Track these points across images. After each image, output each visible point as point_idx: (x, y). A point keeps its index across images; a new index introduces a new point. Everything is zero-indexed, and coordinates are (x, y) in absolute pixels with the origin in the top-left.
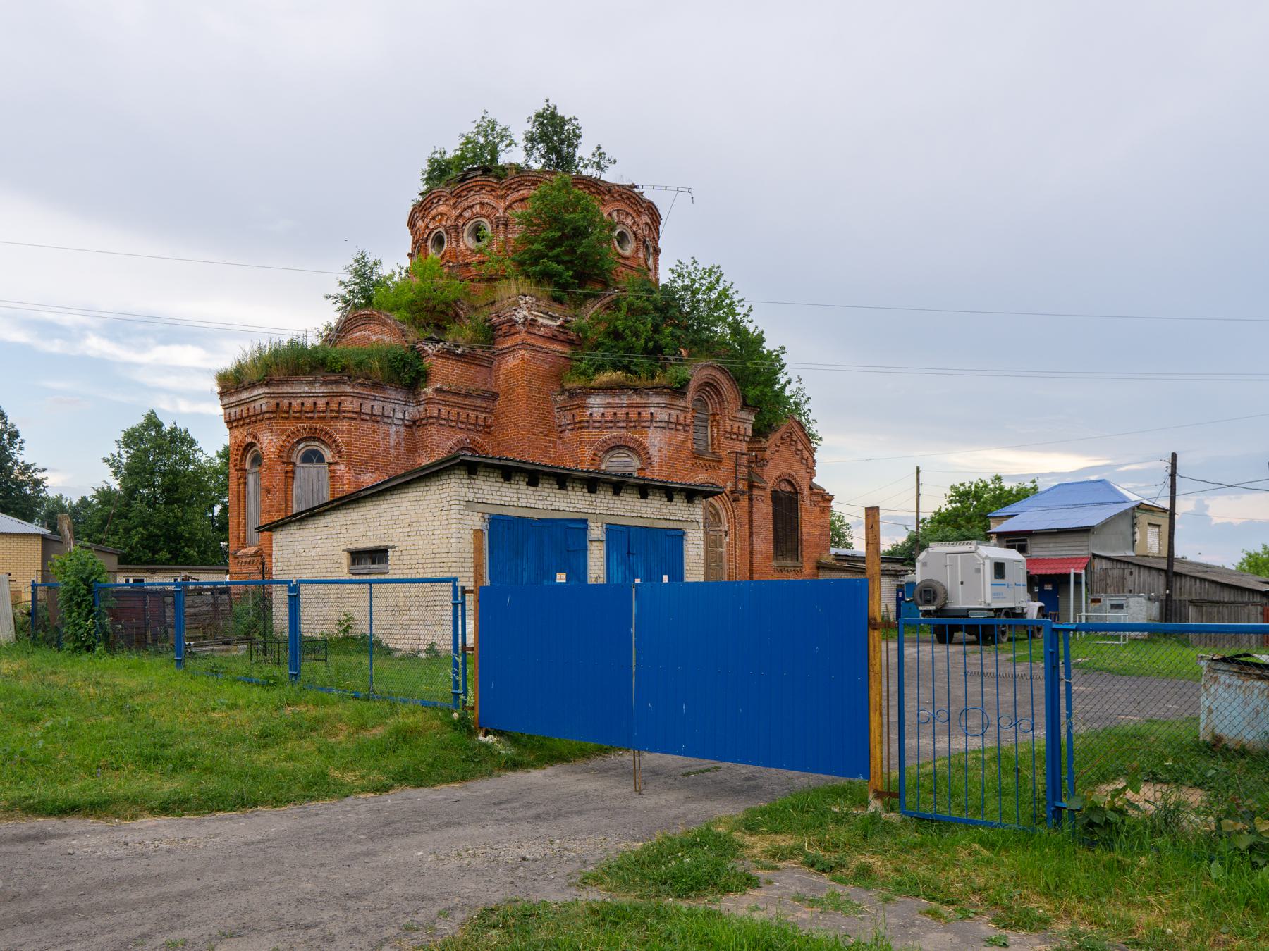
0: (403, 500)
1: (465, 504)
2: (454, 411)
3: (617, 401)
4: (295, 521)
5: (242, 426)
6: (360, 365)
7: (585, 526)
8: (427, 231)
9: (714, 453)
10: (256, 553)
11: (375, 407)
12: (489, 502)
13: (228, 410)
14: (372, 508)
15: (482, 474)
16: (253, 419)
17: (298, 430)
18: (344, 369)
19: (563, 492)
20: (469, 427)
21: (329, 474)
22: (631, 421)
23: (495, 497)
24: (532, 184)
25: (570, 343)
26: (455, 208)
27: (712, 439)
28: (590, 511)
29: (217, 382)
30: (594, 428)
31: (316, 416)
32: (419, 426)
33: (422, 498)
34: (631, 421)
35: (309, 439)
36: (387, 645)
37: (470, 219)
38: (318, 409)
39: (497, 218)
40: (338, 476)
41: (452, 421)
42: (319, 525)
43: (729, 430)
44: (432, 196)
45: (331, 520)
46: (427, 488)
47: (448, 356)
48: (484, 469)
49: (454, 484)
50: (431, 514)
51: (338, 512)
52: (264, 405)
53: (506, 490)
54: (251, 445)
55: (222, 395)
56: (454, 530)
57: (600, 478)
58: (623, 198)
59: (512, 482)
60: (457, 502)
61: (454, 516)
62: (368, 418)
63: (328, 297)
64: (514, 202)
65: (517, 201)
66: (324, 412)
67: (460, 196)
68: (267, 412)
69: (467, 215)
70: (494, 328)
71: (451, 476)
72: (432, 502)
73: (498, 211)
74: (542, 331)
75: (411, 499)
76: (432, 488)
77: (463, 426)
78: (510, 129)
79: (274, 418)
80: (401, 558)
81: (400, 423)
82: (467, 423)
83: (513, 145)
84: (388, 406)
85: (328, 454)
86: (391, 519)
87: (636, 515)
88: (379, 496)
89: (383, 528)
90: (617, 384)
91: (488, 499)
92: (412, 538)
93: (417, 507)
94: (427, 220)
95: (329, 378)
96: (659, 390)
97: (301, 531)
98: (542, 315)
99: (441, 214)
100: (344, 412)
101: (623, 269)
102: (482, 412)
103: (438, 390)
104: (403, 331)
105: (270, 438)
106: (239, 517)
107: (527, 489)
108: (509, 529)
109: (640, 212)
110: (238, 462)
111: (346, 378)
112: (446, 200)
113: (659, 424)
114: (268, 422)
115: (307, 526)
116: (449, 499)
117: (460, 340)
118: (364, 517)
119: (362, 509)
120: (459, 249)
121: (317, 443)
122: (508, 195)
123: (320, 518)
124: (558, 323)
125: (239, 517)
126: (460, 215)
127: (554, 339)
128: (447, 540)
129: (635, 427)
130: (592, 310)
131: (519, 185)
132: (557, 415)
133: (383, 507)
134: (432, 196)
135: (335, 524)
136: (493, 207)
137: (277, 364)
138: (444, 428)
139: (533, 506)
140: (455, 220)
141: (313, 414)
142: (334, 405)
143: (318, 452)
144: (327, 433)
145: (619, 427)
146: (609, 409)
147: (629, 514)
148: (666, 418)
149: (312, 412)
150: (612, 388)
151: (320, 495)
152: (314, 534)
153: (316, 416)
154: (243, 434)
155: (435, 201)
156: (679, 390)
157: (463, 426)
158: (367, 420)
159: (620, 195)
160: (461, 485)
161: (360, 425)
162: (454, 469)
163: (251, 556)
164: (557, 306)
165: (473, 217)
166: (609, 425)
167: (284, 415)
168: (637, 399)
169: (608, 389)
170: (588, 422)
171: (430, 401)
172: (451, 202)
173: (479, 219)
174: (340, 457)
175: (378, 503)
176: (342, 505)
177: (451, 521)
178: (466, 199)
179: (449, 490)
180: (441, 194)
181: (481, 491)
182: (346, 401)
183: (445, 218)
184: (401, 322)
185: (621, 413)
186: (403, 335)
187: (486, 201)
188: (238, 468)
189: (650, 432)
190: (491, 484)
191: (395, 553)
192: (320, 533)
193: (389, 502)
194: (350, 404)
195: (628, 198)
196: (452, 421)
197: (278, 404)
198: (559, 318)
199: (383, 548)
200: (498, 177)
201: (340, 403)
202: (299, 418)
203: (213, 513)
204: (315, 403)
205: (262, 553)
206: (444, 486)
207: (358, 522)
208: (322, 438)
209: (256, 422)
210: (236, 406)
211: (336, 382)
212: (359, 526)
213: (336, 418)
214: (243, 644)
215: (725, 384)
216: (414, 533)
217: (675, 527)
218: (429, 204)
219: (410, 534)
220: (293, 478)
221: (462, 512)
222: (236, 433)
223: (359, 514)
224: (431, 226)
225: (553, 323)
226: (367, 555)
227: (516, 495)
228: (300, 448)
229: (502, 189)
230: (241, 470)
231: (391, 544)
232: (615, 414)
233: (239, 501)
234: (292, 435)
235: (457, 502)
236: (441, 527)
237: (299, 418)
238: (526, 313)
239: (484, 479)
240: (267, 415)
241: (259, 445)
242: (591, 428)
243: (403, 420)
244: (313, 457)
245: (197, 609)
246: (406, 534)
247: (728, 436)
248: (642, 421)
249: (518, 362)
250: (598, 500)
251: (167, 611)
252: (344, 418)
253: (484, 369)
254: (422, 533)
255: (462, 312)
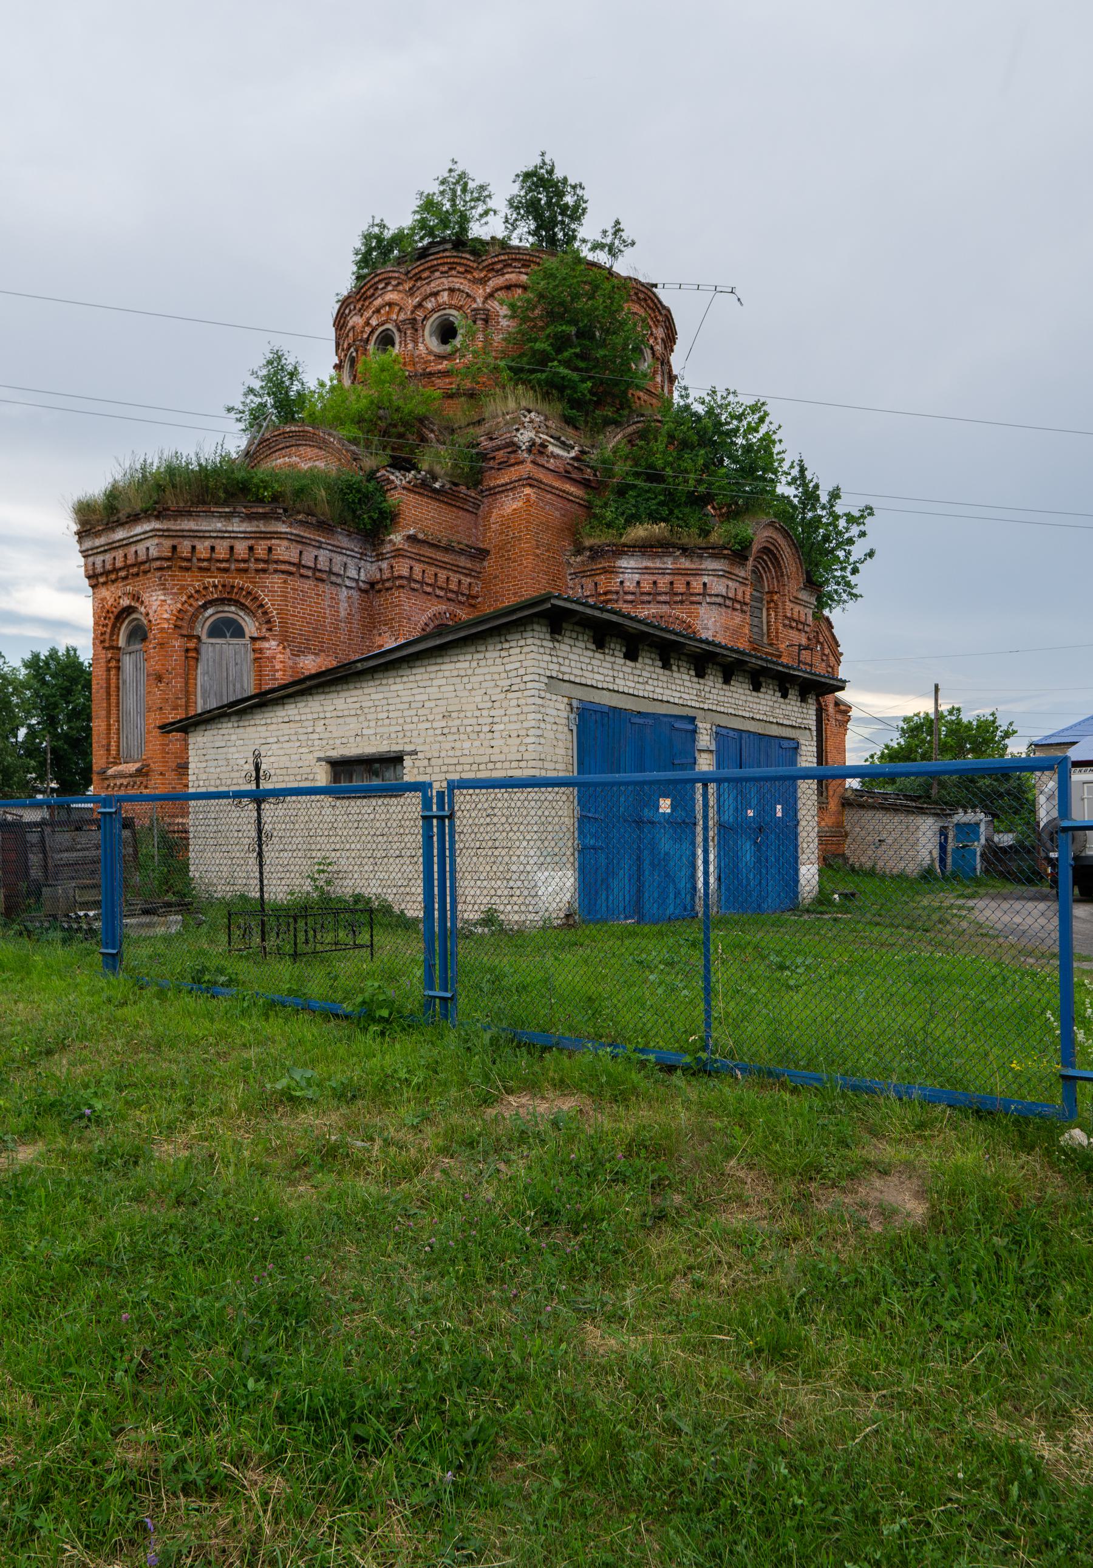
0: (433, 676)
1: (546, 680)
2: (430, 571)
3: (658, 565)
4: (229, 715)
5: (113, 582)
6: (300, 492)
7: (691, 727)
8: (368, 330)
9: (771, 645)
10: (139, 771)
11: (320, 559)
12: (577, 680)
13: (91, 559)
14: (373, 690)
15: (568, 634)
16: (135, 570)
17: (206, 588)
18: (275, 498)
19: (667, 672)
20: (450, 595)
21: (252, 656)
22: (676, 594)
23: (586, 674)
24: (524, 266)
25: (585, 484)
26: (412, 295)
27: (769, 626)
28: (697, 705)
29: (73, 515)
30: (626, 601)
31: (233, 567)
32: (380, 591)
33: (470, 672)
34: (676, 594)
35: (221, 601)
36: (402, 912)
37: (434, 311)
38: (236, 556)
39: (474, 310)
40: (267, 658)
41: (427, 584)
42: (274, 720)
43: (789, 615)
44: (376, 279)
45: (296, 711)
46: (480, 656)
47: (421, 491)
48: (570, 628)
49: (533, 648)
50: (487, 698)
51: (310, 698)
52: (153, 548)
53: (599, 663)
54: (129, 610)
55: (81, 535)
56: (533, 723)
57: (718, 654)
58: (639, 298)
59: (607, 651)
60: (536, 677)
61: (531, 701)
62: (310, 573)
63: (230, 410)
64: (497, 290)
65: (501, 289)
66: (245, 561)
67: (420, 278)
68: (157, 559)
69: (429, 305)
70: (483, 457)
71: (525, 635)
72: (488, 677)
73: (474, 300)
74: (552, 463)
75: (447, 674)
76: (488, 655)
77: (442, 593)
78: (489, 188)
79: (169, 567)
80: (429, 770)
81: (354, 585)
82: (447, 590)
83: (492, 213)
84: (338, 559)
85: (250, 627)
86: (410, 708)
87: (747, 715)
88: (303, 695)
89: (394, 722)
90: (658, 541)
91: (576, 676)
92: (450, 737)
93: (460, 687)
94: (367, 314)
95: (254, 510)
96: (716, 551)
97: (241, 730)
98: (552, 440)
99: (390, 304)
100: (277, 562)
101: (641, 394)
102: (466, 575)
103: (411, 539)
104: (354, 453)
105: (162, 598)
106: (108, 717)
107: (625, 664)
108: (603, 725)
109: (658, 321)
110: (107, 636)
111: (281, 511)
112: (399, 284)
113: (714, 599)
114: (158, 574)
115: (252, 722)
116: (522, 671)
117: (438, 469)
118: (358, 705)
119: (359, 692)
120: (417, 353)
121: (233, 609)
122: (490, 279)
123: (276, 708)
124: (573, 454)
125: (108, 717)
126: (420, 305)
127: (566, 476)
128: (519, 740)
129: (682, 602)
130: (614, 440)
131: (505, 266)
132: (571, 584)
133: (394, 688)
134: (376, 279)
135: (304, 717)
136: (468, 295)
137: (174, 486)
138: (416, 594)
139: (631, 691)
140: (413, 312)
141: (230, 563)
142: (261, 551)
143: (234, 621)
144: (249, 593)
145: (658, 602)
146: (646, 577)
147: (740, 713)
148: (724, 592)
149: (227, 561)
150: (652, 547)
151: (238, 686)
152: (263, 735)
153: (233, 567)
154: (116, 595)
155: (381, 286)
156: (739, 554)
157: (442, 593)
158: (307, 577)
159: (636, 294)
160: (542, 650)
161: (299, 583)
162: (532, 623)
163: (131, 776)
164: (570, 430)
165: (438, 308)
166: (646, 598)
167: (184, 564)
168: (685, 563)
169: (645, 548)
170: (617, 593)
171: (398, 553)
172: (407, 286)
173: (447, 311)
174: (270, 630)
175: (384, 682)
176: (317, 686)
177: (526, 709)
178: (428, 284)
179: (522, 657)
180: (391, 275)
181: (567, 662)
182: (279, 546)
183: (397, 309)
184: (349, 441)
185: (663, 582)
186: (355, 460)
187: (457, 286)
188: (107, 645)
189: (702, 610)
190: (579, 651)
191: (418, 763)
192: (274, 734)
193: (405, 679)
194: (285, 551)
195: (645, 299)
196: (427, 584)
197: (174, 548)
198: (573, 448)
199: (393, 755)
200: (475, 253)
201: (270, 549)
202: (208, 570)
203: (16, 737)
204: (232, 548)
205: (149, 771)
206: (512, 651)
207: (346, 713)
208: (243, 601)
209: (137, 575)
210: (105, 551)
211: (264, 517)
212: (348, 720)
213: (264, 571)
214: (177, 913)
215: (787, 553)
216: (454, 730)
217: (788, 735)
218: (372, 291)
219: (446, 731)
220: (197, 659)
221: (543, 694)
222: (104, 592)
223: (349, 700)
224: (374, 322)
225: (565, 454)
226: (362, 768)
227: (611, 673)
228: (207, 614)
229: (481, 270)
230: (111, 648)
231: (409, 748)
232: (655, 583)
233: (108, 694)
234: (196, 596)
235: (536, 677)
236: (506, 719)
237: (208, 570)
238: (532, 434)
239: (572, 642)
240: (158, 564)
241: (142, 610)
242: (621, 602)
243: (357, 581)
244: (226, 629)
245: (80, 854)
246: (439, 732)
247: (787, 622)
248: (692, 594)
249: (520, 504)
250: (707, 689)
251: (31, 856)
252: (276, 571)
253: (468, 515)
254: (469, 729)
255: (432, 435)
